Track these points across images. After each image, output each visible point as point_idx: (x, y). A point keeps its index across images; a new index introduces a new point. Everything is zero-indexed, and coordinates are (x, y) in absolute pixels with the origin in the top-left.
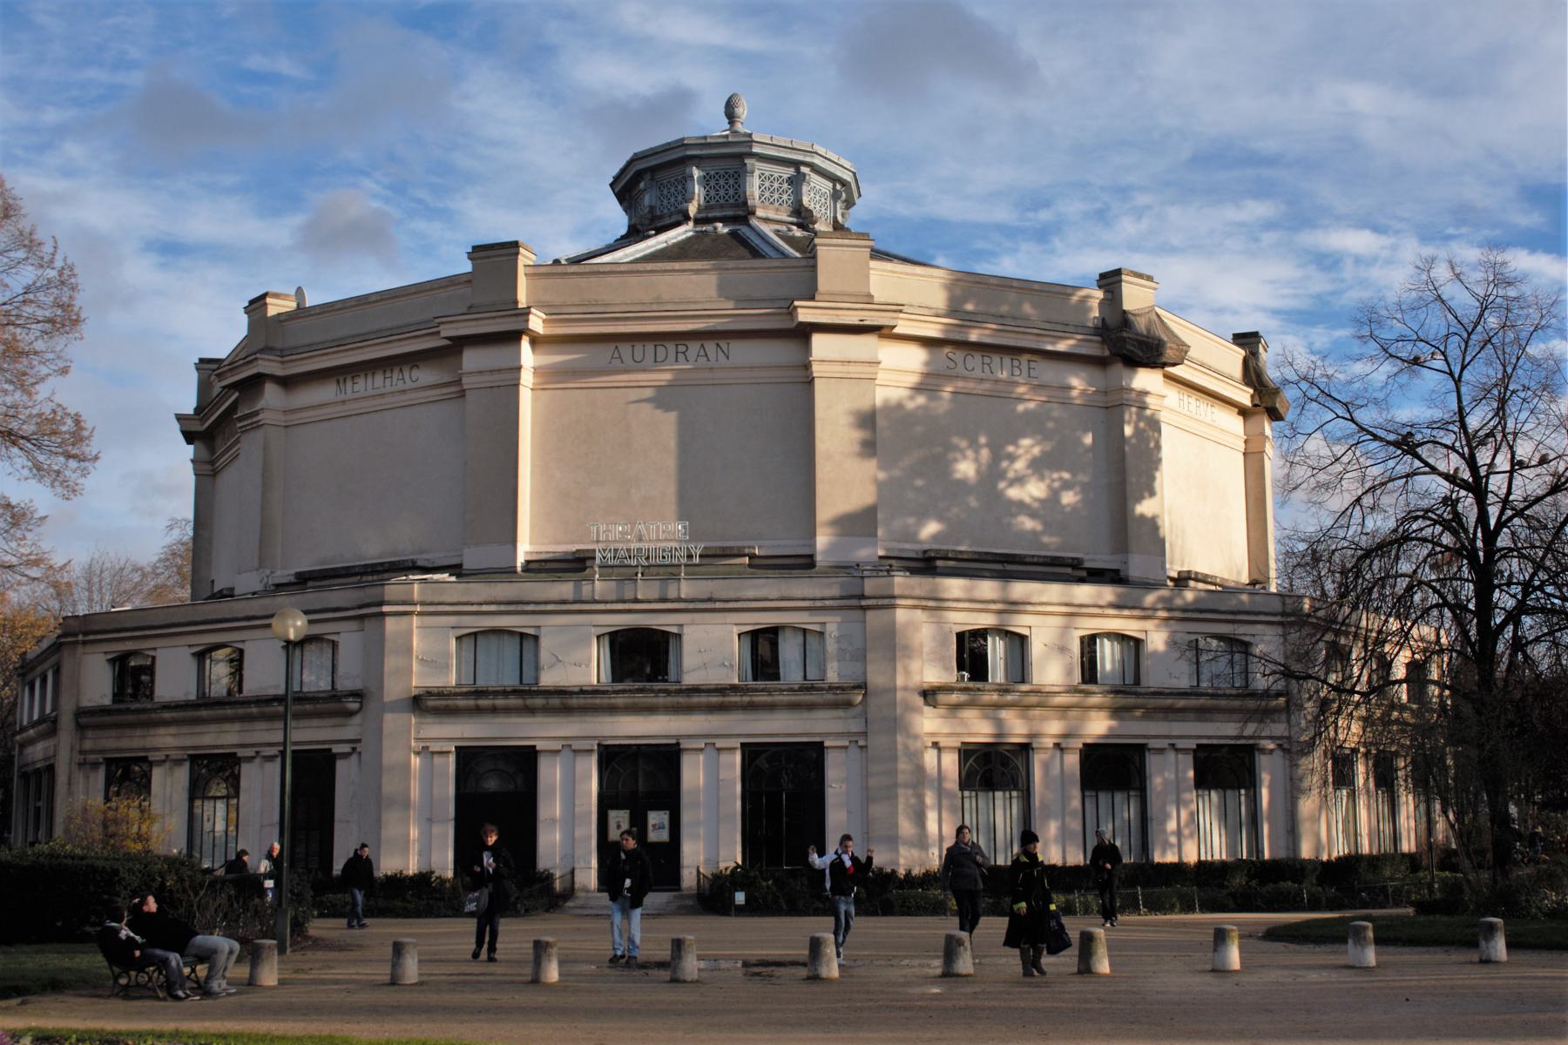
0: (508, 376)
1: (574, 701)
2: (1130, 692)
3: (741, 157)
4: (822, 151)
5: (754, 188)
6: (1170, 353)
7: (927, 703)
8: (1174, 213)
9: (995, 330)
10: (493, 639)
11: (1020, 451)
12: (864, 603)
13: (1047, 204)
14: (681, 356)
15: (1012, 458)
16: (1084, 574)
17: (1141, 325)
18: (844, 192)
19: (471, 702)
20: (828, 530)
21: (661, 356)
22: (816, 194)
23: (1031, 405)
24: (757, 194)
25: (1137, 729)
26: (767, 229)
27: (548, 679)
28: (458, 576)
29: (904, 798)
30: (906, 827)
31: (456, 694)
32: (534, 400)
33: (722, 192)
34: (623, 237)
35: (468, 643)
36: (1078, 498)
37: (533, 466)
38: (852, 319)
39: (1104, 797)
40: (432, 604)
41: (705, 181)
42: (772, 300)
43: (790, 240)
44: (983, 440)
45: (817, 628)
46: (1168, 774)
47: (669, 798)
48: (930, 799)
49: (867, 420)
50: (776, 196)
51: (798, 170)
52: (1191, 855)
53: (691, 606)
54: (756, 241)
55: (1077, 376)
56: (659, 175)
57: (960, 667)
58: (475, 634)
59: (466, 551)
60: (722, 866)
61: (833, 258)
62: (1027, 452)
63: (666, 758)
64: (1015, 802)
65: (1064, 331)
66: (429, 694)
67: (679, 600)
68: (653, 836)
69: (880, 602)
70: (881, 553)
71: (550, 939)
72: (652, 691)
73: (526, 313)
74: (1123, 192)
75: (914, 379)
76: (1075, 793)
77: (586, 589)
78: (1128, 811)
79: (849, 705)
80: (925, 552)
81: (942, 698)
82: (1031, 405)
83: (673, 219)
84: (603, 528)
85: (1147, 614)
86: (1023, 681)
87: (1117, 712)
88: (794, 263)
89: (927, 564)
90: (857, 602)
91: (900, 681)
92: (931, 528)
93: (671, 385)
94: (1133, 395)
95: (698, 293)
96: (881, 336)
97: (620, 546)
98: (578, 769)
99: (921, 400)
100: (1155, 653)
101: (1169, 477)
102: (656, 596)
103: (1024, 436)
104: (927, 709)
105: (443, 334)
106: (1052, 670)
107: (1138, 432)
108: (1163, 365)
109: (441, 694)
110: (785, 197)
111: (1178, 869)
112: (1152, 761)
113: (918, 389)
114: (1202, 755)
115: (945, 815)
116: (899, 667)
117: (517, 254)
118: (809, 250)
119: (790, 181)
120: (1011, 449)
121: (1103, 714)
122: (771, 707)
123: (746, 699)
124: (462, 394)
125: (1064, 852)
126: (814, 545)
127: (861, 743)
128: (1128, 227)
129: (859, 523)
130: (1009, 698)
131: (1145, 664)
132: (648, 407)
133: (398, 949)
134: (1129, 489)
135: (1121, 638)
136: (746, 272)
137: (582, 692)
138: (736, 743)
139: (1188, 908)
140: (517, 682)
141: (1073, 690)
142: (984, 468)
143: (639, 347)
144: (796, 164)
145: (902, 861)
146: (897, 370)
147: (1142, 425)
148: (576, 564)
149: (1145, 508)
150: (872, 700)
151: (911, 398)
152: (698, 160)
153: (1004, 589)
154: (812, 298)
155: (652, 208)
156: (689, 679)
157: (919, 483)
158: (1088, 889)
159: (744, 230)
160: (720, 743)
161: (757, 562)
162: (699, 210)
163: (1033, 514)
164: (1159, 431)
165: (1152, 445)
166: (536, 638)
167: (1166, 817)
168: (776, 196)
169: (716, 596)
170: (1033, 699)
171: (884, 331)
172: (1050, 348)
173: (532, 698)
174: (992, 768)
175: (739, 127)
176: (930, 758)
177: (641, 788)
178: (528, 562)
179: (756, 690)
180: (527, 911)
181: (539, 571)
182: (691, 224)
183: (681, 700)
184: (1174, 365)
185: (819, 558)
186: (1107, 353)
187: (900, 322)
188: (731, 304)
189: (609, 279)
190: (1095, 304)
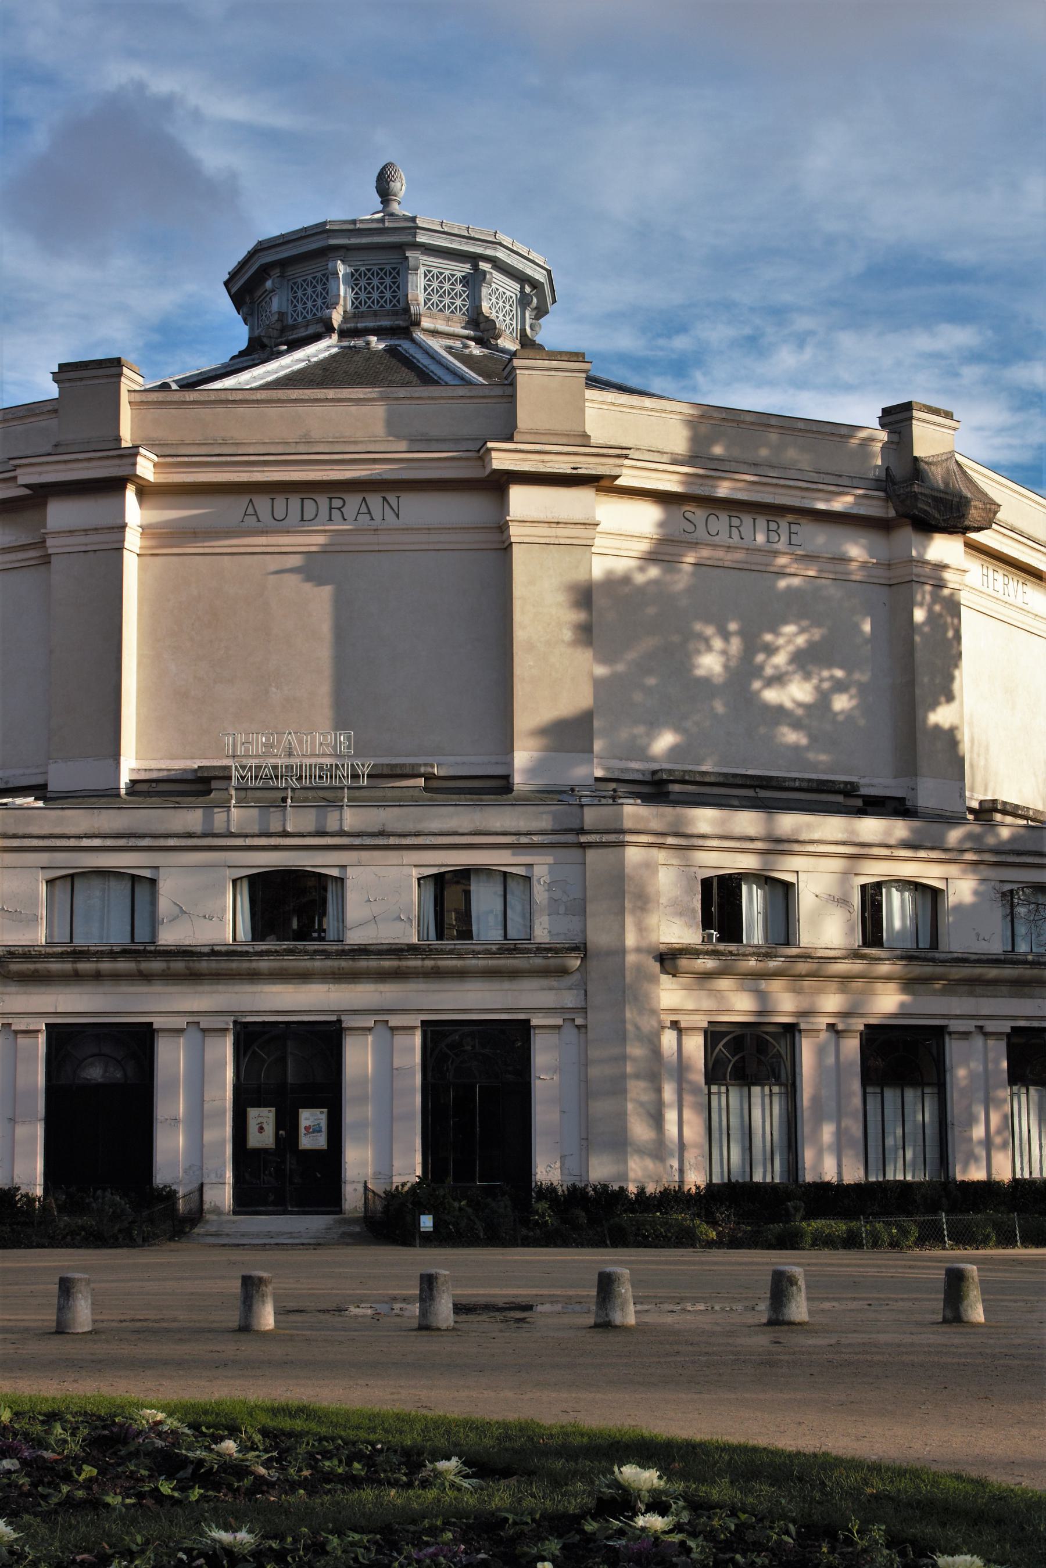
0: (114, 537)
1: (204, 965)
2: (927, 956)
3: (400, 248)
4: (507, 241)
5: (417, 290)
6: (974, 514)
7: (665, 971)
8: (847, 340)
9: (746, 482)
10: (96, 883)
11: (781, 641)
12: (583, 839)
13: (683, 329)
14: (336, 513)
15: (771, 650)
16: (859, 803)
17: (937, 475)
18: (535, 296)
19: (68, 966)
20: (533, 743)
21: (309, 514)
22: (498, 298)
23: (796, 581)
24: (422, 299)
25: (936, 1006)
26: (436, 345)
27: (169, 936)
28: (45, 799)
29: (637, 1090)
30: (640, 1130)
31: (48, 955)
32: (142, 569)
33: (375, 295)
34: (242, 354)
35: (62, 892)
36: (854, 702)
37: (141, 657)
38: (561, 465)
39: (891, 1095)
40: (15, 836)
41: (354, 279)
42: (457, 440)
43: (468, 360)
44: (733, 626)
45: (521, 871)
46: (972, 1064)
47: (328, 1093)
48: (669, 1093)
49: (585, 596)
50: (447, 301)
51: (475, 267)
52: (1003, 1171)
53: (357, 841)
54: (424, 361)
55: (856, 543)
56: (290, 272)
57: (707, 923)
58: (72, 876)
59: (53, 768)
60: (397, 1180)
61: (532, 382)
62: (789, 642)
63: (325, 1039)
64: (776, 1100)
65: (841, 485)
66: (12, 954)
67: (341, 833)
68: (306, 1142)
69: (605, 838)
70: (599, 773)
71: (264, 1274)
72: (306, 952)
73: (132, 453)
74: (779, 313)
75: (644, 546)
76: (856, 1085)
77: (219, 818)
78: (922, 1112)
79: (563, 972)
80: (654, 773)
81: (684, 963)
82: (796, 581)
83: (311, 330)
84: (241, 738)
85: (953, 856)
86: (787, 943)
87: (909, 984)
88: (480, 392)
89: (656, 789)
90: (572, 839)
91: (631, 940)
92: (665, 741)
93: (324, 551)
94: (927, 570)
95: (359, 427)
96: (600, 490)
97: (262, 762)
98: (209, 1056)
99: (654, 572)
100: (959, 908)
101: (968, 678)
102: (311, 828)
103: (786, 622)
104: (665, 978)
105: (21, 481)
106: (826, 929)
107: (932, 618)
108: (964, 530)
109: (27, 954)
110: (458, 302)
111: (989, 1189)
112: (953, 1048)
113: (651, 558)
114: (1015, 1040)
115: (687, 1114)
116: (629, 921)
117: (120, 375)
118: (502, 376)
119: (465, 280)
120: (768, 637)
121: (892, 986)
122: (461, 974)
123: (429, 963)
124: (46, 560)
125: (839, 1166)
126: (510, 764)
127: (579, 1021)
128: (787, 359)
129: (570, 734)
130: (773, 964)
131: (947, 920)
132: (293, 579)
133: (66, 1287)
134: (918, 691)
135: (917, 887)
136: (424, 405)
137: (214, 953)
138: (415, 1020)
139: (1007, 1240)
140: (128, 941)
141: (855, 955)
142: (733, 663)
143: (280, 502)
144: (474, 259)
145: (632, 1175)
146: (622, 533)
147: (937, 608)
148: (199, 786)
149: (941, 716)
150: (592, 964)
151: (642, 569)
152: (344, 252)
153: (770, 822)
154: (510, 439)
155: (282, 315)
156: (354, 938)
157: (651, 681)
158: (875, 1215)
159: (405, 345)
160: (395, 1021)
161: (435, 784)
162: (346, 318)
163: (796, 724)
164: (958, 615)
165: (950, 634)
166: (153, 882)
167: (971, 1120)
168: (447, 301)
169: (389, 829)
170: (802, 967)
171: (603, 483)
172: (821, 506)
173: (148, 959)
174: (750, 1055)
175: (395, 208)
176: (668, 1039)
177: (290, 1080)
178: (133, 782)
179: (441, 952)
180: (144, 1240)
181: (148, 794)
182: (335, 337)
183: (344, 964)
184: (978, 529)
185: (518, 779)
186: (892, 513)
187: (625, 471)
188: (403, 446)
189: (241, 410)
190: (877, 447)
